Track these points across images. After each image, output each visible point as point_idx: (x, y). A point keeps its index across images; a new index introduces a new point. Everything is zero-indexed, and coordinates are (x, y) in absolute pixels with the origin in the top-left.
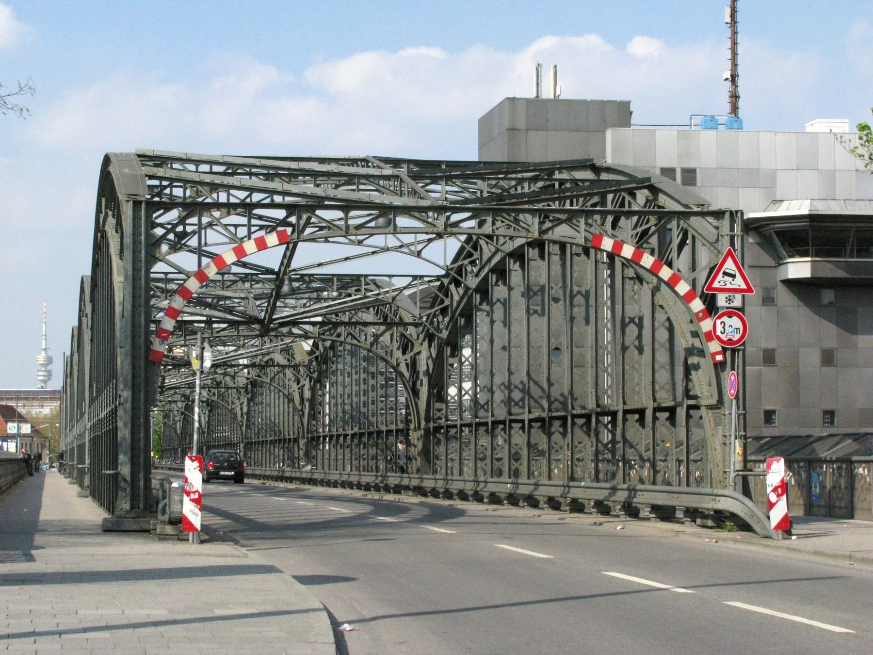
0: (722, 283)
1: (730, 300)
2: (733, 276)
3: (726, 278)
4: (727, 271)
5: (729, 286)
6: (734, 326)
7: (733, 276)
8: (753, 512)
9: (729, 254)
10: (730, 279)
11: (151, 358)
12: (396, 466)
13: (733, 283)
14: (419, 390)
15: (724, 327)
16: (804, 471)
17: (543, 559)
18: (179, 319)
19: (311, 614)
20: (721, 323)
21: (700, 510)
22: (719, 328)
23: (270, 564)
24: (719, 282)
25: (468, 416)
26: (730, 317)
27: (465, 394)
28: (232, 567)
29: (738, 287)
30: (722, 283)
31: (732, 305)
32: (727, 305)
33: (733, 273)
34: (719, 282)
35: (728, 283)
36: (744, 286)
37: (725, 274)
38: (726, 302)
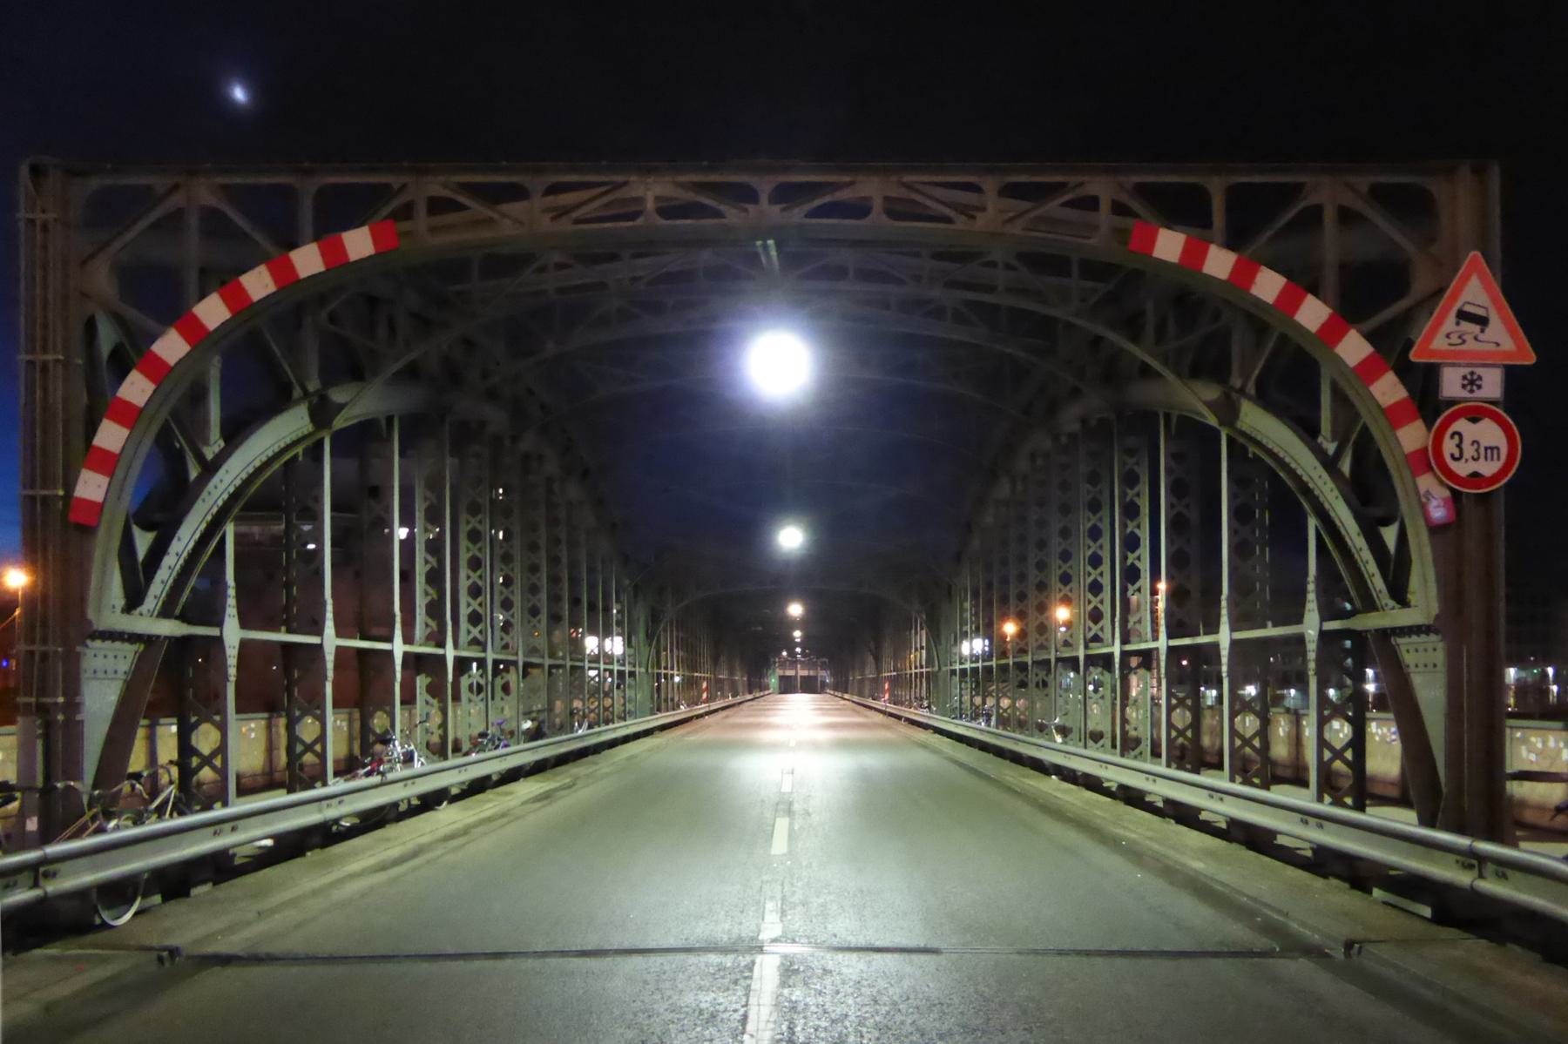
0: (1455, 340)
2: (1482, 321)
3: (1467, 326)
4: (1468, 308)
6: (1484, 443)
7: (1482, 321)
10: (1476, 328)
11: (72, 517)
13: (1481, 337)
14: (763, 687)
15: (1459, 446)
19: (861, 941)
21: (1148, 799)
22: (1449, 446)
23: (327, 850)
24: (1448, 336)
26: (1474, 420)
28: (685, 719)
30: (1455, 340)
31: (1478, 394)
33: (1481, 312)
34: (1448, 336)
38: (1480, 378)
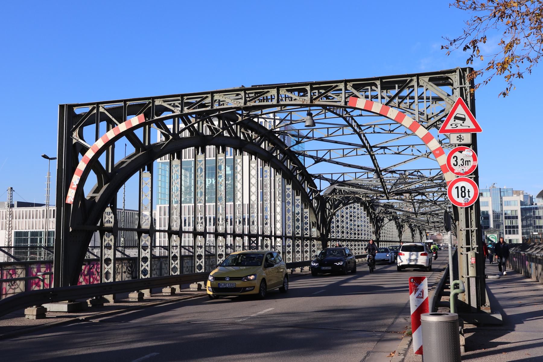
1: (460, 138)
2: (463, 120)
3: (457, 121)
4: (458, 115)
5: (460, 127)
8: (277, 277)
9: (459, 102)
12: (195, 133)
16: (5, 267)
17: (194, 334)
18: (446, 270)
20: (454, 158)
25: (29, 244)
27: (252, 243)
29: (468, 128)
31: (463, 142)
32: (458, 142)
33: (463, 117)
34: (451, 125)
35: (459, 125)
36: (473, 127)
37: (456, 118)
38: (458, 140)
